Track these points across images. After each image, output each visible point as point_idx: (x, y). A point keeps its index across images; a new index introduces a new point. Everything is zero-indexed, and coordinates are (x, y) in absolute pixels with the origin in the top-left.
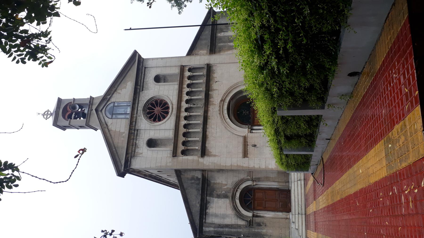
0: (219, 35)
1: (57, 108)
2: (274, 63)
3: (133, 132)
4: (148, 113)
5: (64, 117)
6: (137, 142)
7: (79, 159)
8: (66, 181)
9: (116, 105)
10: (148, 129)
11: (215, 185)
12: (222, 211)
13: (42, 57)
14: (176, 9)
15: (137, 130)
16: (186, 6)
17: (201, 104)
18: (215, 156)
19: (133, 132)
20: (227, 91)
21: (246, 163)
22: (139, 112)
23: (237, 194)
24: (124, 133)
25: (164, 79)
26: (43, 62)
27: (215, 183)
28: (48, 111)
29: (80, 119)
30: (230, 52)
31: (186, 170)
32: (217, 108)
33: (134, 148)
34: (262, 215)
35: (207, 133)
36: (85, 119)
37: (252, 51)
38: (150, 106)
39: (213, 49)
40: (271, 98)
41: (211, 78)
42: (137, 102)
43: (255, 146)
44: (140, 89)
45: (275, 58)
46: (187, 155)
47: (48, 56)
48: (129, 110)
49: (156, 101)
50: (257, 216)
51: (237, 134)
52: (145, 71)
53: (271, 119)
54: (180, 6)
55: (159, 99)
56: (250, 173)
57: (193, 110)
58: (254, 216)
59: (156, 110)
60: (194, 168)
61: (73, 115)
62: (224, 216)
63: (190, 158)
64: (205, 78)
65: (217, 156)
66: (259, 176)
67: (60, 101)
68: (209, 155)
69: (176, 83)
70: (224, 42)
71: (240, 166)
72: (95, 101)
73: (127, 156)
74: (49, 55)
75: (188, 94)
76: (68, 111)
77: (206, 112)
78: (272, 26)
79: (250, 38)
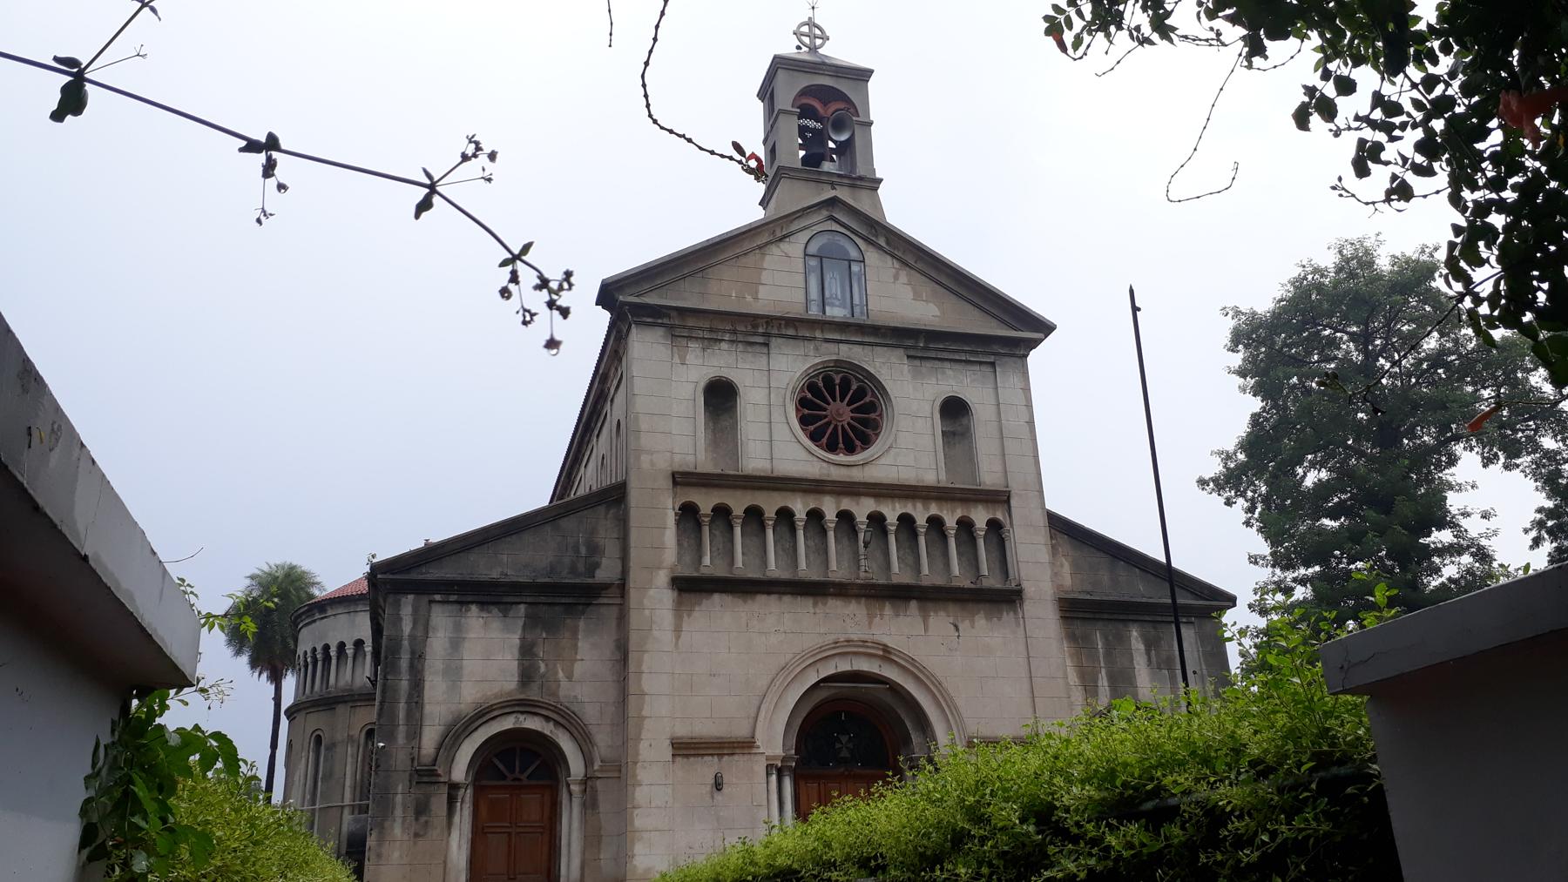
0: (1135, 634)
1: (837, 66)
2: (1072, 867)
3: (761, 330)
4: (828, 381)
5: (807, 92)
6: (724, 346)
7: (731, 158)
8: (650, 116)
9: (855, 268)
10: (770, 384)
11: (567, 635)
12: (473, 663)
13: (1080, 14)
14: (1215, 468)
15: (767, 345)
16: (1229, 503)
17: (869, 570)
18: (678, 630)
19: (759, 330)
20: (922, 669)
21: (652, 749)
22: (832, 346)
23: (536, 719)
24: (756, 299)
25: (954, 434)
26: (1062, 18)
27: (575, 633)
28: (825, 38)
29: (801, 147)
30: (1073, 678)
31: (623, 523)
32: (856, 634)
33: (701, 334)
34: (457, 819)
35: (762, 598)
36: (799, 165)
37: (1112, 774)
38: (854, 387)
39: (1078, 612)
40: (922, 855)
41: (970, 605)
42: (866, 339)
43: (718, 785)
44: (914, 348)
45: (1091, 871)
46: (678, 523)
47: (1085, 35)
48: (836, 312)
49: (872, 407)
50: (451, 801)
51: (761, 717)
52: (981, 363)
53: (837, 854)
54: (1227, 482)
55: (881, 415)
56: (615, 772)
57: (845, 541)
58: (454, 787)
59: (840, 409)
60: (633, 553)
61: (811, 124)
62: (453, 673)
63: (670, 535)
64: (967, 584)
65: (678, 638)
66: (604, 806)
67: (863, 75)
68: (679, 609)
69: (943, 476)
70: (1109, 653)
71: (640, 728)
72: (864, 194)
73: (673, 314)
74: (1087, 38)
75: (906, 521)
76: (825, 104)
77: (841, 591)
78: (1219, 857)
79: (1160, 765)
